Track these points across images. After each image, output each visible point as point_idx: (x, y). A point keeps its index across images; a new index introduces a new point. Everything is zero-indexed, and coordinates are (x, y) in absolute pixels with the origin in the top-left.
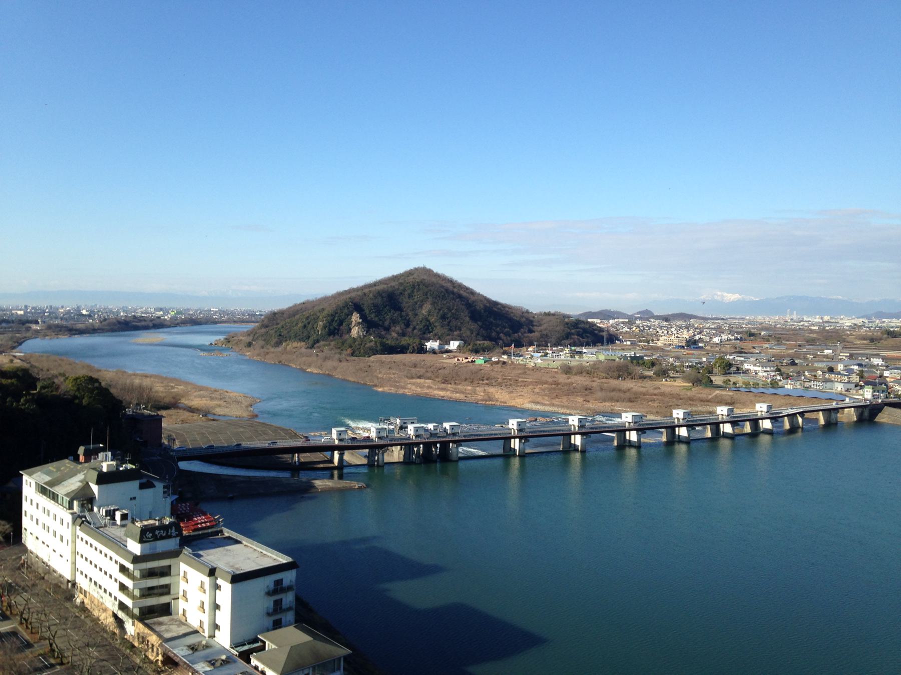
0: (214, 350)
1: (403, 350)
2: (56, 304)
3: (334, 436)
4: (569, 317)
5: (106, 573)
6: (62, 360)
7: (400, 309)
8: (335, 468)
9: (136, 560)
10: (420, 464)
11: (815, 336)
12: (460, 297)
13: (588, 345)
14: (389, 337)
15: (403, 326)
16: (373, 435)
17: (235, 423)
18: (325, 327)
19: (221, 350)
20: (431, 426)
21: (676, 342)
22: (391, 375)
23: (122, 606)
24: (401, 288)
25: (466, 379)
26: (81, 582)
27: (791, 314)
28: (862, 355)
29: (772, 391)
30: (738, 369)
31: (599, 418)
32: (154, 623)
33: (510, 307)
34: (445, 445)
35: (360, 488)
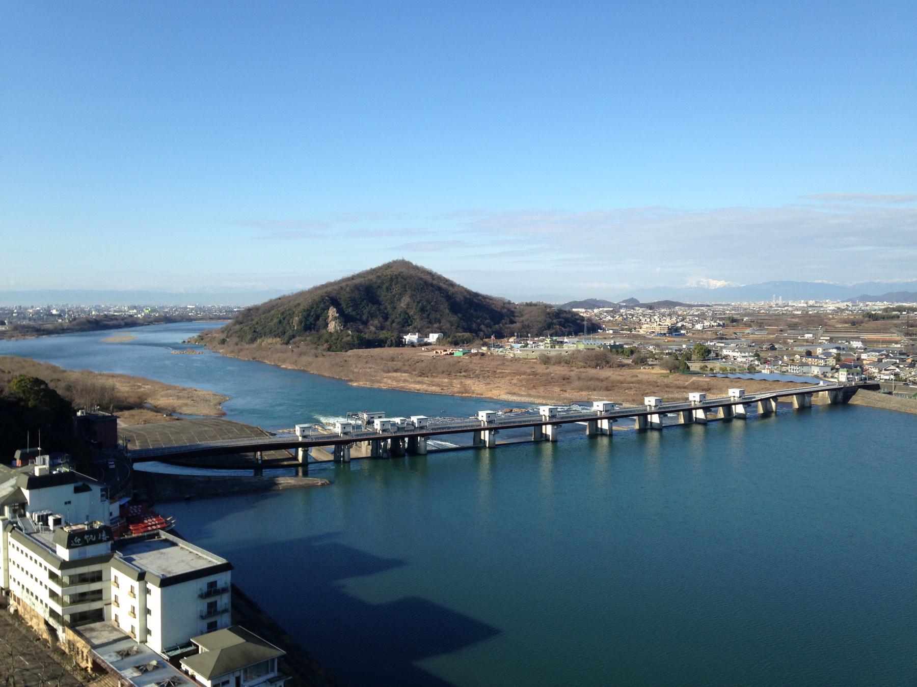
0: (185, 348)
1: (380, 344)
2: (25, 303)
3: (298, 433)
4: (550, 307)
5: (36, 580)
6: (25, 361)
9: (64, 565)
10: (388, 458)
11: (797, 320)
12: (439, 289)
13: (569, 334)
14: (366, 330)
15: (381, 319)
16: (338, 430)
17: (199, 422)
18: (300, 322)
19: (193, 348)
20: (397, 420)
21: (658, 329)
22: (368, 369)
23: (53, 613)
24: (379, 281)
25: (443, 372)
26: (15, 589)
27: (777, 298)
28: (842, 338)
29: (749, 376)
30: (717, 355)
31: (575, 407)
32: (86, 630)
33: (491, 298)
34: (413, 438)
35: (323, 485)
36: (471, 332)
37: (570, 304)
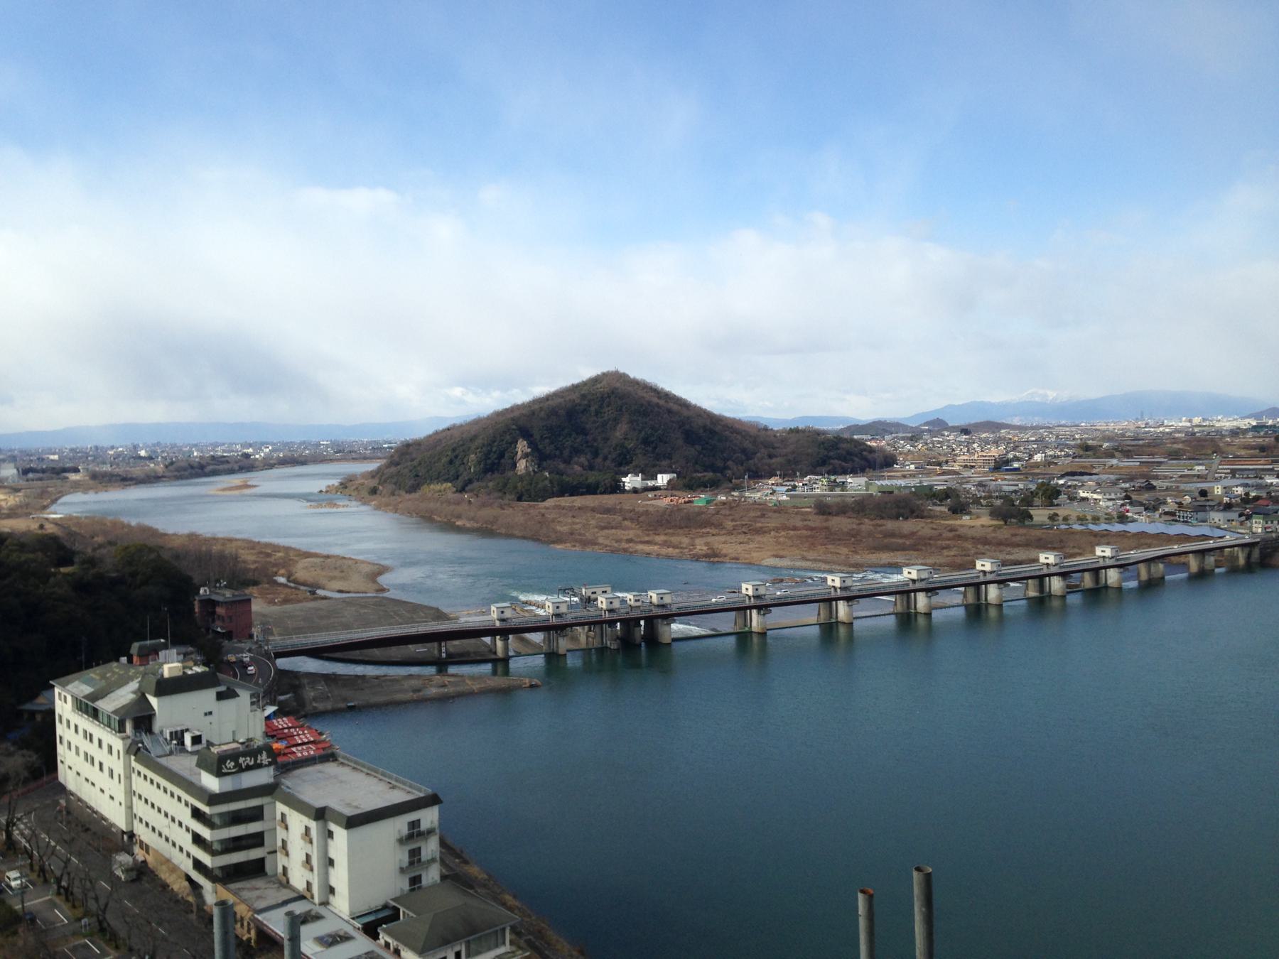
1: (592, 490)
7: (584, 432)
8: (499, 660)
11: (1180, 446)
23: (198, 865)
26: (140, 830)
29: (1118, 527)
33: (739, 422)
36: (714, 471)
37: (849, 428)
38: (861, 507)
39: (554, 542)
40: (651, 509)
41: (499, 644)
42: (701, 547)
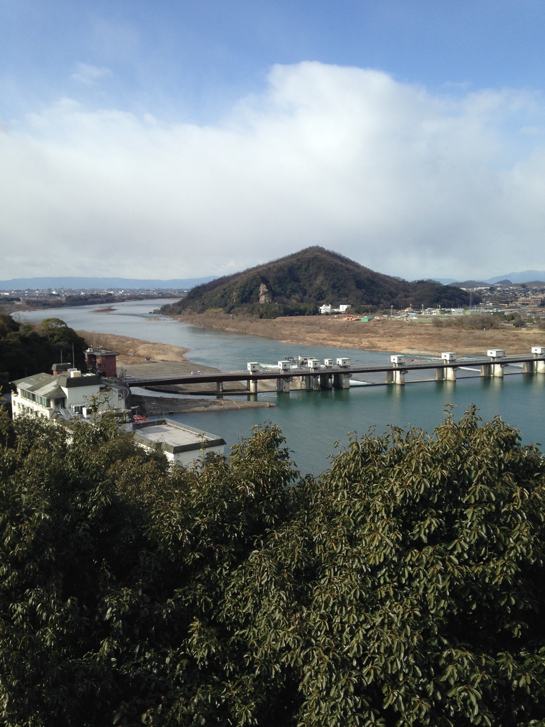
1: (302, 313)
3: (249, 369)
7: (298, 280)
8: (251, 394)
15: (301, 294)
36: (372, 304)
38: (460, 323)
39: (281, 339)
40: (336, 323)
41: (252, 385)
42: (365, 343)
